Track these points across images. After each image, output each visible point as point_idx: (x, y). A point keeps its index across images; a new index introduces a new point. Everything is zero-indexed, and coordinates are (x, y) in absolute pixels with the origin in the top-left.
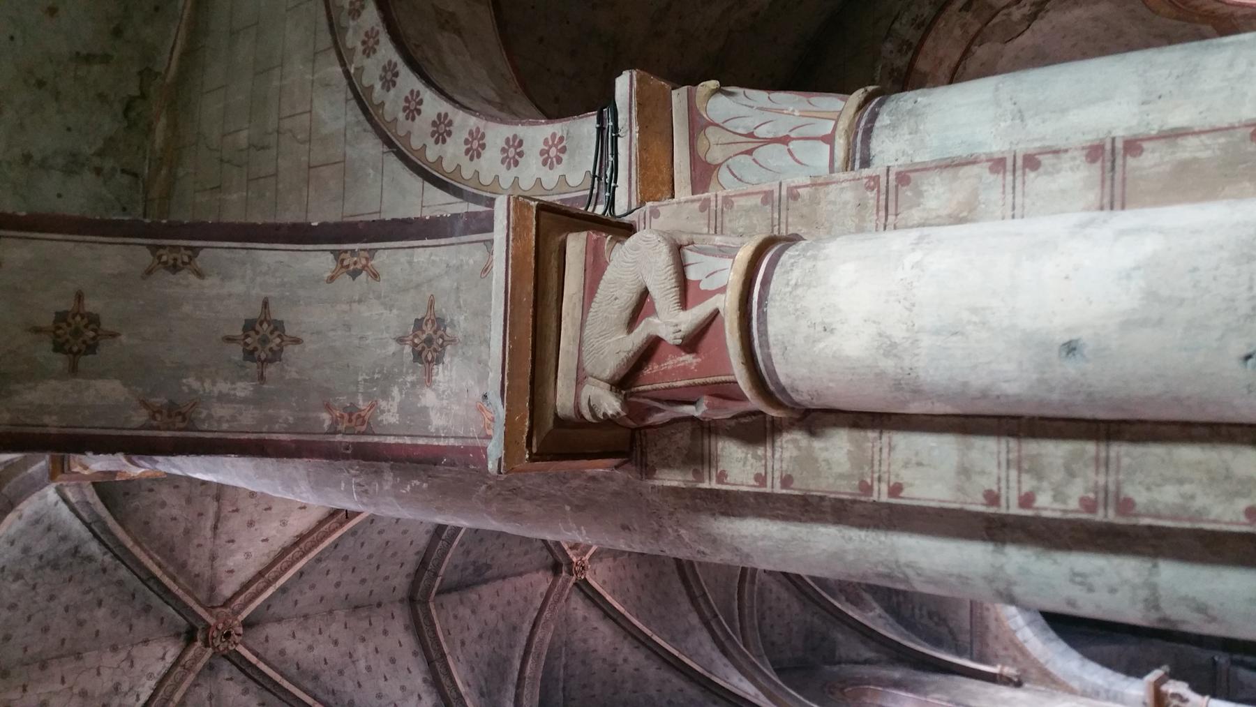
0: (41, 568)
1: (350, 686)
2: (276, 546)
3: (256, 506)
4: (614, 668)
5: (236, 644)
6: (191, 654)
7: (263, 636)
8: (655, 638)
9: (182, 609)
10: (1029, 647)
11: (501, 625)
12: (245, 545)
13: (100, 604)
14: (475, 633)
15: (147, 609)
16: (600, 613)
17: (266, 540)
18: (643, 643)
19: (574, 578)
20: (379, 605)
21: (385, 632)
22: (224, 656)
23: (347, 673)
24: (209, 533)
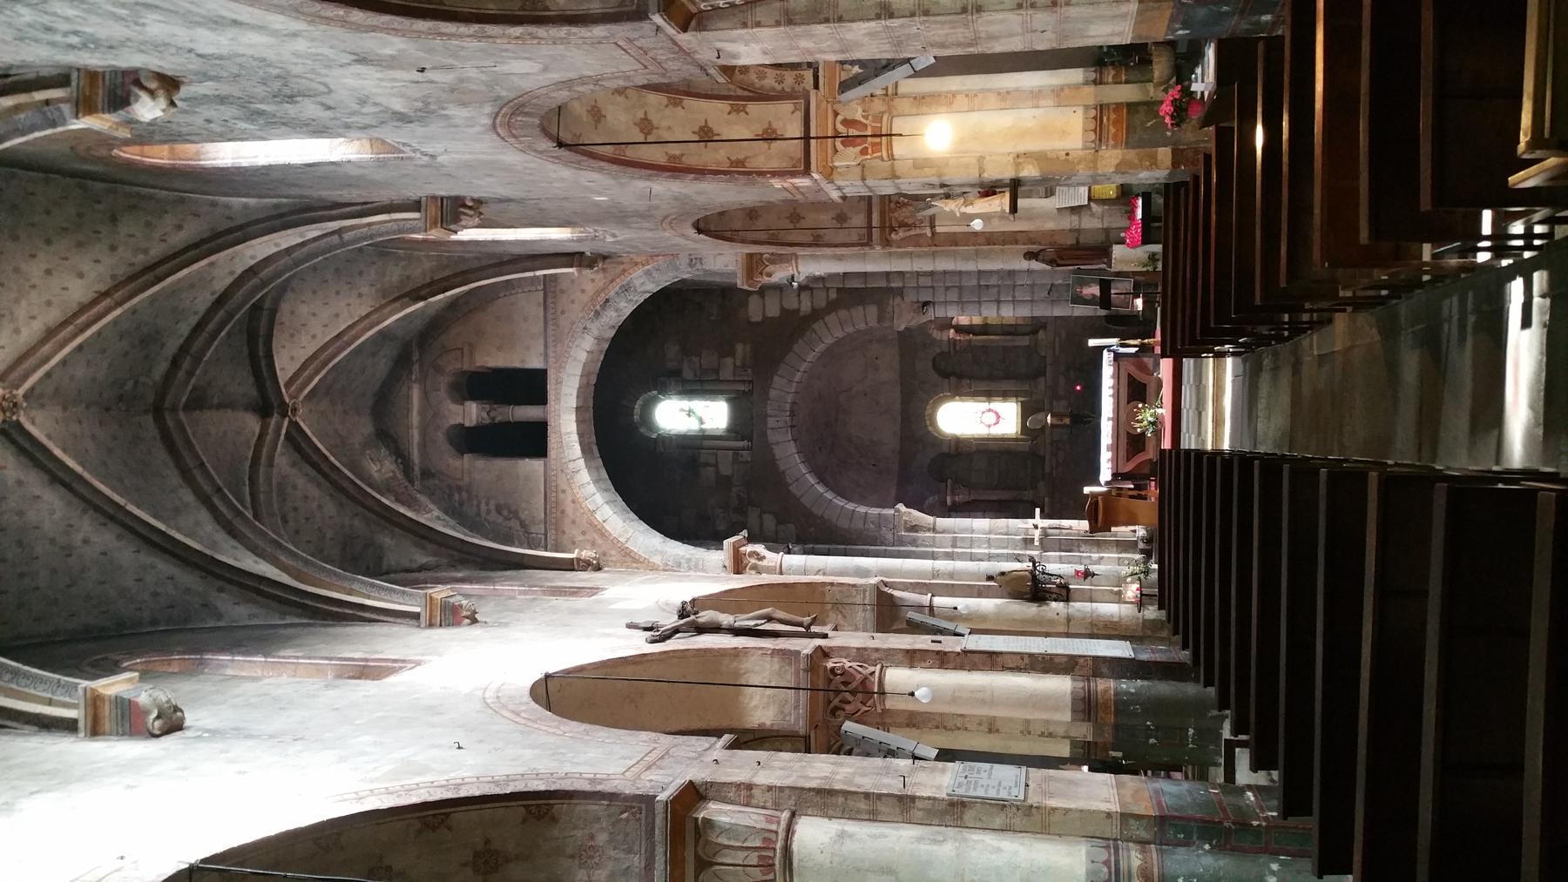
4: (68, 551)
8: (131, 508)
16: (46, 477)
18: (112, 518)
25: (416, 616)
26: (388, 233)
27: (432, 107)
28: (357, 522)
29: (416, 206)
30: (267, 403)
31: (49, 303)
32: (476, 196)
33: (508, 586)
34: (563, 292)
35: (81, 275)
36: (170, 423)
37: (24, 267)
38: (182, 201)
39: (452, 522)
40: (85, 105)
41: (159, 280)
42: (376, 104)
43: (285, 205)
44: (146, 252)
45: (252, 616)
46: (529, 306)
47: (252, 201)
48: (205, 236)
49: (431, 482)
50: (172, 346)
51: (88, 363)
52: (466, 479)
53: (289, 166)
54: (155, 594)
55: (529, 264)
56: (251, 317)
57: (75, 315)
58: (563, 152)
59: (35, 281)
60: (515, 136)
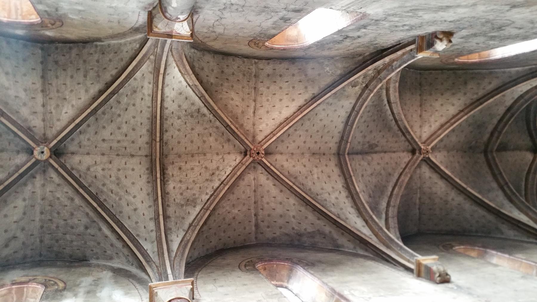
0: (187, 115)
1: (310, 184)
2: (278, 122)
3: (269, 105)
4: (446, 202)
6: (245, 159)
7: (274, 159)
8: (469, 189)
9: (242, 142)
11: (383, 172)
12: (266, 120)
14: (369, 172)
15: (229, 140)
16: (439, 176)
17: (274, 119)
18: (462, 192)
19: (422, 156)
20: (324, 154)
21: (326, 165)
22: (258, 163)
23: (309, 178)
24: (252, 115)
31: (442, 116)
35: (453, 105)
36: (490, 157)
37: (433, 104)
38: (491, 73)
40: (420, 49)
43: (534, 68)
44: (477, 94)
45: (515, 236)
48: (500, 85)
50: (490, 128)
51: (457, 136)
53: (524, 54)
57: (451, 119)
59: (437, 109)
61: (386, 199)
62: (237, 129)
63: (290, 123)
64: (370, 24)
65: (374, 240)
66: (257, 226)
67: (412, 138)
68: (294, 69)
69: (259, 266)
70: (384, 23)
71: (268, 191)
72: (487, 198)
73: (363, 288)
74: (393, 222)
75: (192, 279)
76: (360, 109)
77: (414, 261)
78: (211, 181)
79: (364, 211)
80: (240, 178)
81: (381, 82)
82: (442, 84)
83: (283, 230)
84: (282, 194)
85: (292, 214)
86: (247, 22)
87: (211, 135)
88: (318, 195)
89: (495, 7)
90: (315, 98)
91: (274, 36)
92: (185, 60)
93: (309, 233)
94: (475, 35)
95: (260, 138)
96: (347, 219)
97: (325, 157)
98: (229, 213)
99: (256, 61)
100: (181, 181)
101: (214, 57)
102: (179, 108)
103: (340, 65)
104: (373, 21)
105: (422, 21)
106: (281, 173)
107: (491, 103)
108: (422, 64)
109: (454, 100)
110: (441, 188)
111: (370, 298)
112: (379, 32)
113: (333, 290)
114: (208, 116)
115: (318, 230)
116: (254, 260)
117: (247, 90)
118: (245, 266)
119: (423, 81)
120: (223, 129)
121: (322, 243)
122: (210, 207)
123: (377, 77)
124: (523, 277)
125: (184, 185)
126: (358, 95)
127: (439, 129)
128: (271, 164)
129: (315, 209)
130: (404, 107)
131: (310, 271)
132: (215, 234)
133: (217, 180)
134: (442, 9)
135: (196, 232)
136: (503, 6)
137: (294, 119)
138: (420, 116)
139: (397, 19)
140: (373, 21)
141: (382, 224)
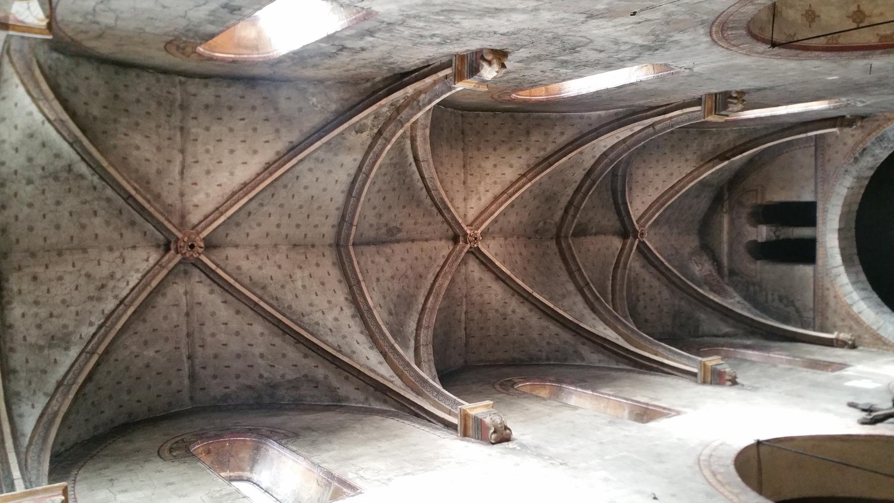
0: (45, 177)
1: (289, 297)
2: (228, 191)
3: (211, 159)
5: (199, 254)
6: (166, 257)
7: (224, 256)
8: (535, 294)
9: (159, 226)
10: (863, 317)
11: (409, 272)
13: (95, 213)
14: (389, 274)
15: (133, 223)
17: (220, 185)
18: (527, 299)
19: (468, 246)
20: (313, 246)
21: (318, 265)
22: (194, 264)
23: (287, 287)
24: (178, 177)
25: (694, 375)
26: (682, 122)
27: (662, 37)
28: (683, 303)
29: (698, 102)
30: (626, 231)
31: (495, 183)
32: (738, 89)
33: (779, 355)
34: (829, 146)
35: (511, 166)
36: (564, 245)
37: (483, 164)
38: (564, 118)
39: (748, 305)
40: (459, 76)
41: (551, 165)
42: (626, 43)
43: (620, 113)
44: (545, 149)
45: (600, 361)
46: (804, 158)
47: (602, 113)
49: (735, 278)
50: (564, 201)
52: (759, 277)
53: (608, 91)
54: (548, 343)
55: (803, 128)
56: (611, 182)
57: (508, 189)
58: (776, 50)
59: (488, 171)
60: (734, 46)
61: (416, 316)
62: (149, 202)
63: (250, 192)
64: (379, 30)
65: (397, 385)
66: (192, 376)
67: (454, 218)
68: (254, 98)
69: (197, 448)
70: (401, 28)
71: (213, 314)
72: (562, 307)
73: (380, 465)
74: (426, 353)
75: (64, 484)
76: (371, 170)
77: (457, 412)
78: (99, 299)
79: (382, 337)
80: (158, 292)
81: (402, 126)
82: (495, 133)
83: (243, 381)
84: (239, 317)
85: (257, 350)
86: (159, 9)
87: (95, 213)
88: (303, 316)
89: (566, 15)
90: (293, 150)
91: (212, 36)
92: (38, 72)
93: (289, 381)
94: (539, 58)
95: (194, 218)
96: (354, 352)
97: (313, 250)
98: (136, 356)
99: (183, 79)
100: (36, 303)
101: (98, 69)
102: (28, 164)
103: (334, 95)
104: (384, 25)
105: (459, 30)
106: (236, 280)
107: (564, 164)
108: (465, 100)
109: (512, 158)
110: (496, 295)
111: (389, 480)
112: (395, 43)
113: (330, 474)
114: (90, 177)
115: (306, 376)
116: (187, 438)
117: (165, 132)
118: (171, 450)
119: (470, 125)
120: (121, 202)
121: (312, 397)
122: (97, 347)
123: (395, 119)
124: (611, 423)
125: (44, 310)
126: (366, 147)
127: (492, 204)
128: (217, 265)
129: (299, 339)
130: (440, 168)
131: (290, 447)
132: (110, 397)
133: (110, 298)
134: (489, 12)
135: (71, 396)
136: (576, 15)
137: (258, 185)
138: (464, 183)
139: (421, 24)
140: (384, 25)
141: (409, 357)
